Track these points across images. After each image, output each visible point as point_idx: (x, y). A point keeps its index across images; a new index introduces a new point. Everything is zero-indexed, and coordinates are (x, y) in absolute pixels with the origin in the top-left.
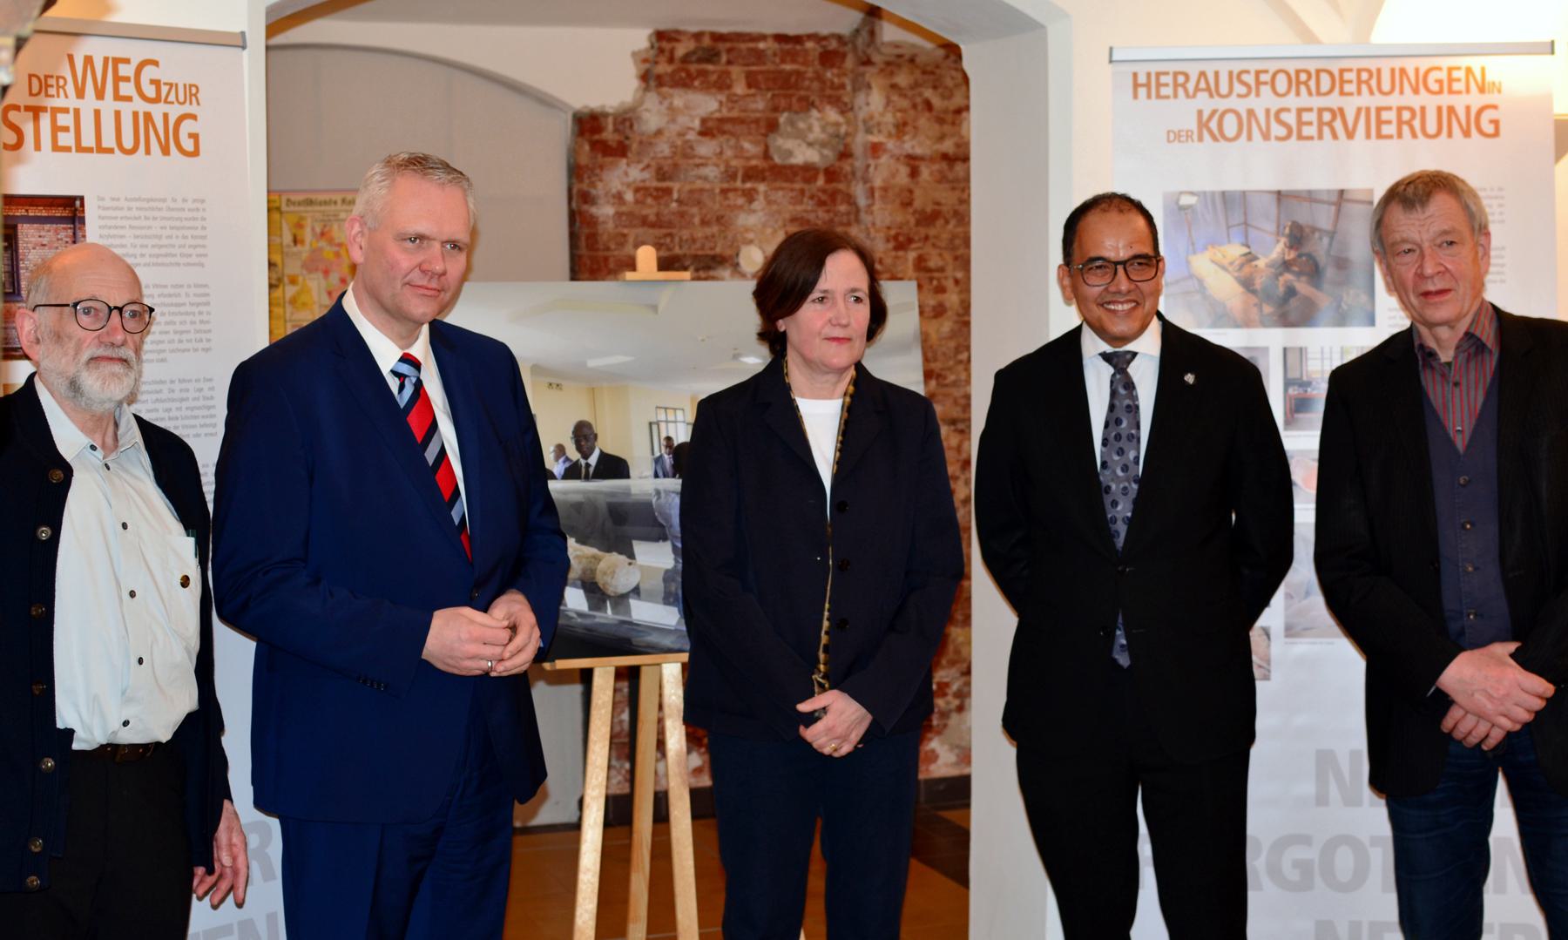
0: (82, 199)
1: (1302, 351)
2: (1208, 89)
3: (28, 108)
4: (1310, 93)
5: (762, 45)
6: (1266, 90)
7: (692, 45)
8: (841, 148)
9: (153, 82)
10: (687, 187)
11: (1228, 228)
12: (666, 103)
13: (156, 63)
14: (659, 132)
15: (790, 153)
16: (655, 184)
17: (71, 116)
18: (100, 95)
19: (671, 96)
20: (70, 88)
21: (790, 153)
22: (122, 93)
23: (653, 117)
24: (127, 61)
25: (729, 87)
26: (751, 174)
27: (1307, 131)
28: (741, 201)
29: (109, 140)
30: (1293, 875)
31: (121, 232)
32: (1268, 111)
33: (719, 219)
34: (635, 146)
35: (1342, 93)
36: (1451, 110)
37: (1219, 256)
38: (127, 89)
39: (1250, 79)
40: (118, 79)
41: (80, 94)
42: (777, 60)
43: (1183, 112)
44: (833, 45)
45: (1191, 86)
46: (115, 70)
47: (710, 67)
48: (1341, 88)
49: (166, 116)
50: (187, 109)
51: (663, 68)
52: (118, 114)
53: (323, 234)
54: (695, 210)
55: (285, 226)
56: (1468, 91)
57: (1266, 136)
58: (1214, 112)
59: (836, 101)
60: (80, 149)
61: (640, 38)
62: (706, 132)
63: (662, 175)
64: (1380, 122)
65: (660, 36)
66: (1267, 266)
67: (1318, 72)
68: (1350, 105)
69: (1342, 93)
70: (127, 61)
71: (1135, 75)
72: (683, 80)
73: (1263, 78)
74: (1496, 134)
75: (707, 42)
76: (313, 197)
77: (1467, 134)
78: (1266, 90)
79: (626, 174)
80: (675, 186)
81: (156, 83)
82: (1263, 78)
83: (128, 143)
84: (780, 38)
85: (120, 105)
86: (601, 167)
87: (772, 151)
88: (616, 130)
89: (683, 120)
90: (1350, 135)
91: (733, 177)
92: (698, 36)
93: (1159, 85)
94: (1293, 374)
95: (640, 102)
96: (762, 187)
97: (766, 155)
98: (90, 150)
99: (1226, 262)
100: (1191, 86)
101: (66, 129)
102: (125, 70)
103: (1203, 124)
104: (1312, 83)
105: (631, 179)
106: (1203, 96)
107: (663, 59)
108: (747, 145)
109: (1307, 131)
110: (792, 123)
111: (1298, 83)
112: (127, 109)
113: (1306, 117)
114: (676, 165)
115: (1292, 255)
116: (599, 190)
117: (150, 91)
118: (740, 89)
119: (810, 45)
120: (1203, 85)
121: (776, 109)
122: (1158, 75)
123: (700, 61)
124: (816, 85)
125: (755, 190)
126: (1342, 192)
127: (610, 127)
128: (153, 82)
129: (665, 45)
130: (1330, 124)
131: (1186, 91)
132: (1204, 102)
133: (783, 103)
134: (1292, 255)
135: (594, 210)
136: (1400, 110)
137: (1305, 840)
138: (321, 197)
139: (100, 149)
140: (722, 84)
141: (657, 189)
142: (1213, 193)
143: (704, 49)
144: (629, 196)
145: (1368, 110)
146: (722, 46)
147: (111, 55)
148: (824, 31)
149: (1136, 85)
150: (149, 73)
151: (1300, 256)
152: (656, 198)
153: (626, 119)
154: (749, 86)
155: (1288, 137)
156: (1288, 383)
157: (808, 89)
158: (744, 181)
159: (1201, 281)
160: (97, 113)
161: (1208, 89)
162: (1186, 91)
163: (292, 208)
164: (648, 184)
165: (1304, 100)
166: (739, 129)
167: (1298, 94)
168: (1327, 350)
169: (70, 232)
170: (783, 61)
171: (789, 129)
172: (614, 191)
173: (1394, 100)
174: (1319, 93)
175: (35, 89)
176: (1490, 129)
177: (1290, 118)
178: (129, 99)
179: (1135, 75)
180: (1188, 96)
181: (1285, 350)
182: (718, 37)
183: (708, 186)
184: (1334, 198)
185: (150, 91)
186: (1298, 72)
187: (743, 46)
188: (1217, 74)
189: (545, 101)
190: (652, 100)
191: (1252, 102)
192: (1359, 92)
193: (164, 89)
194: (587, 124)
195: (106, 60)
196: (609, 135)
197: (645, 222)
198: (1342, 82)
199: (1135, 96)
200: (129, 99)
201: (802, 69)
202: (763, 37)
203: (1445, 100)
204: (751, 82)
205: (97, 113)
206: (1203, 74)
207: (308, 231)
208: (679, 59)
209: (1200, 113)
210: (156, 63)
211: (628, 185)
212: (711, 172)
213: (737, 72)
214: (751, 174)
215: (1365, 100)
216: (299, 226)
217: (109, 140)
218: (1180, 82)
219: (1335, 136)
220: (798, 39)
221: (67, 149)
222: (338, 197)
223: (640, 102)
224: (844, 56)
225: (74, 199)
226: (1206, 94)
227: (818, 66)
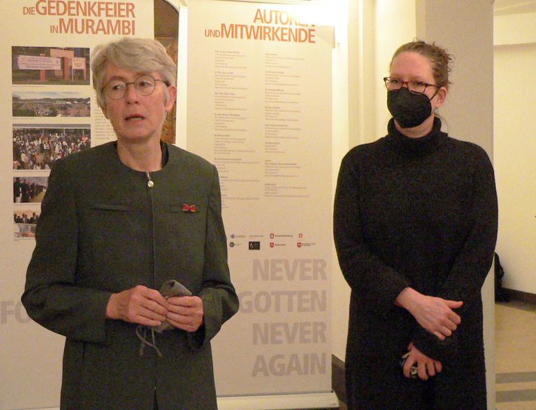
1: (63, 19)
2: (261, 18)
8: (169, 286)
17: (288, 36)
45: (95, 27)
56: (290, 40)
84: (27, 236)
90: (66, 31)
100: (95, 27)
101: (111, 9)
106: (101, 33)
111: (88, 26)
115: (88, 103)
120: (101, 27)
131: (93, 30)
134: (88, 103)
161: (103, 29)
162: (93, 30)
180: (93, 33)
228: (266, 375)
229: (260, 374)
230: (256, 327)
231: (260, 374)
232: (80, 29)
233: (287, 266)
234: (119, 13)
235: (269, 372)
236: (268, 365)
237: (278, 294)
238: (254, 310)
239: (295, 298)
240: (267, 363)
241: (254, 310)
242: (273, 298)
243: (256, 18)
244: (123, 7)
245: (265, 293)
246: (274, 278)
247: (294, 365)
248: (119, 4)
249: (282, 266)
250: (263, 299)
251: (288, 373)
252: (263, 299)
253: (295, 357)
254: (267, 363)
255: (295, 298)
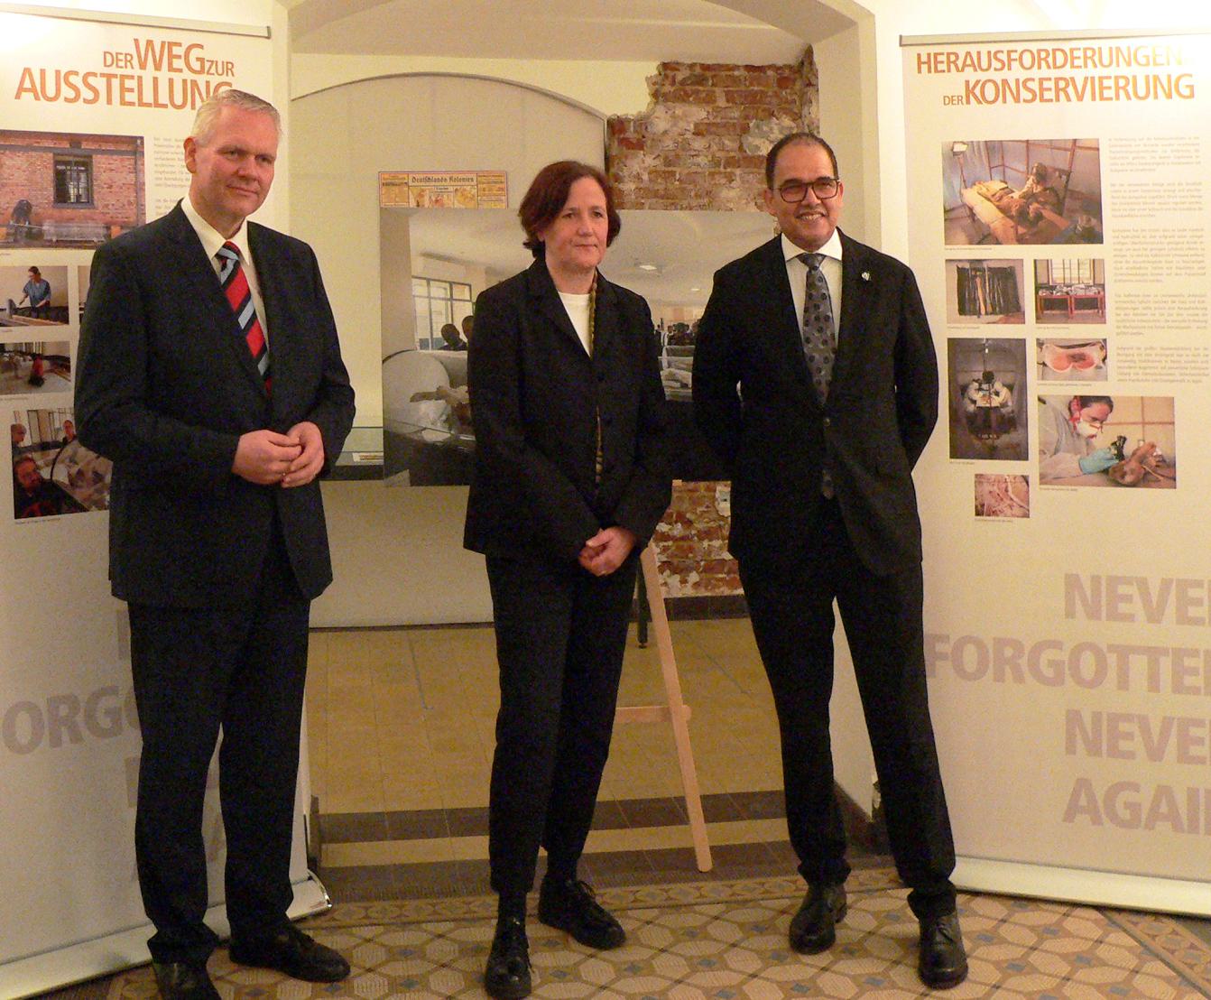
0: (142, 138)
2: (33, 89)
3: (103, 75)
4: (1049, 67)
5: (736, 73)
6: (1015, 65)
7: (687, 73)
9: (198, 59)
10: (686, 171)
11: (991, 168)
12: (670, 112)
13: (201, 46)
14: (665, 132)
15: (758, 148)
16: (663, 168)
18: (158, 67)
19: (675, 107)
20: (135, 62)
21: (758, 148)
22: (175, 66)
23: (661, 123)
24: (180, 45)
25: (715, 101)
26: (730, 162)
27: (1047, 95)
28: (723, 181)
29: (163, 98)
30: (1049, 672)
31: (171, 163)
32: (1017, 81)
33: (708, 193)
34: (649, 143)
35: (1073, 66)
36: (1156, 78)
37: (984, 190)
38: (178, 63)
39: (1004, 57)
40: (171, 56)
41: (143, 66)
42: (747, 83)
43: (954, 82)
44: (787, 73)
45: (960, 63)
46: (170, 51)
47: (701, 88)
48: (1072, 63)
49: (208, 83)
50: (224, 78)
51: (668, 88)
52: (171, 81)
53: (437, 201)
54: (691, 187)
55: (411, 196)
57: (1017, 100)
58: (978, 82)
59: (788, 112)
60: (141, 104)
61: (652, 68)
62: (697, 133)
63: (668, 162)
64: (1102, 88)
65: (665, 66)
66: (1021, 197)
67: (1054, 51)
68: (1079, 75)
69: (1073, 66)
70: (180, 45)
71: (919, 55)
72: (682, 97)
73: (1014, 56)
74: (1192, 95)
75: (698, 70)
76: (430, 176)
77: (1169, 96)
78: (1015, 65)
79: (643, 162)
80: (677, 170)
81: (201, 60)
82: (1014, 56)
83: (179, 101)
84: (749, 68)
85: (173, 75)
86: (626, 157)
87: (745, 147)
88: (636, 131)
89: (682, 124)
90: (1080, 98)
91: (718, 164)
92: (692, 66)
93: (936, 62)
94: (1042, 280)
95: (653, 110)
96: (738, 171)
97: (741, 148)
98: (149, 105)
99: (989, 195)
100: (960, 63)
101: (131, 90)
102: (176, 50)
103: (969, 91)
104: (1050, 60)
105: (646, 165)
107: (667, 83)
108: (727, 142)
109: (1047, 95)
110: (758, 127)
111: (1040, 59)
112: (178, 78)
113: (1046, 84)
114: (677, 156)
115: (1038, 189)
116: (625, 172)
117: (197, 66)
118: (722, 102)
119: (770, 73)
121: (747, 117)
122: (936, 55)
123: (692, 84)
124: (775, 101)
125: (732, 174)
126: (1075, 141)
127: (632, 129)
128: (198, 59)
129: (670, 73)
130: (1064, 90)
132: (971, 75)
133: (752, 113)
135: (621, 186)
136: (1117, 78)
137: (1056, 645)
138: (436, 176)
139: (157, 105)
140: (709, 100)
141: (664, 172)
142: (979, 142)
143: (695, 76)
144: (645, 177)
145: (1093, 78)
146: (709, 74)
147: (168, 39)
148: (780, 63)
149: (920, 63)
150: (195, 53)
151: (1045, 189)
152: (665, 178)
153: (643, 122)
154: (728, 101)
155: (1033, 100)
156: (1038, 288)
157: (770, 103)
158: (725, 168)
159: (971, 209)
160: (155, 80)
163: (416, 184)
164: (658, 169)
165: (1045, 72)
166: (721, 130)
167: (1040, 67)
168: (1067, 262)
169: (133, 162)
170: (751, 84)
171: (756, 131)
172: (635, 173)
173: (1112, 71)
174: (1055, 67)
175: (109, 62)
176: (1187, 92)
177: (1034, 86)
178: (180, 70)
179: (919, 55)
181: (1035, 261)
182: (706, 68)
183: (700, 170)
184: (1069, 145)
185: (197, 66)
186: (1039, 51)
187: (723, 73)
188: (979, 53)
189: (589, 113)
190: (660, 110)
191: (1005, 74)
192: (1086, 66)
193: (207, 65)
194: (616, 127)
195: (163, 43)
196: (631, 134)
197: (656, 195)
198: (1073, 58)
199: (920, 71)
200: (180, 70)
201: (765, 89)
202: (736, 67)
203: (1152, 71)
204: (730, 98)
205: (155, 80)
206: (968, 54)
207: (426, 198)
208: (680, 81)
209: (967, 82)
210: (201, 46)
211: (645, 169)
212: (702, 160)
213: (719, 92)
214: (730, 162)
215: (1091, 71)
216: (421, 195)
217: (163, 98)
218: (952, 60)
219: (1069, 99)
220: (761, 69)
221: (132, 104)
222: (447, 177)
223: (653, 110)
224: (794, 81)
225: (136, 138)
226: (971, 69)
227: (776, 89)
228: (1094, 823)
229: (1083, 819)
230: (1074, 718)
231: (1083, 819)
232: (1142, 92)
233: (1146, 730)
234: (1101, 94)
235: (1104, 816)
236: (1100, 803)
237: (1124, 652)
238: (1069, 681)
239: (1166, 664)
240: (1100, 796)
241: (1069, 681)
242: (1112, 659)
243: (21, 89)
244: (120, 57)
245: (1092, 647)
246: (1114, 616)
247: (1164, 809)
248: (117, 54)
249: (1133, 728)
250: (1088, 661)
251: (1150, 826)
252: (1088, 661)
253: (1164, 792)
254: (1100, 796)
255: (1166, 664)
